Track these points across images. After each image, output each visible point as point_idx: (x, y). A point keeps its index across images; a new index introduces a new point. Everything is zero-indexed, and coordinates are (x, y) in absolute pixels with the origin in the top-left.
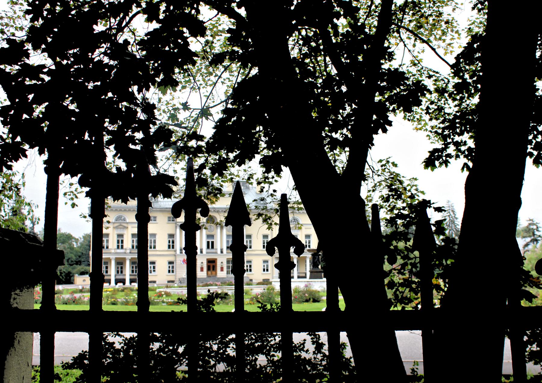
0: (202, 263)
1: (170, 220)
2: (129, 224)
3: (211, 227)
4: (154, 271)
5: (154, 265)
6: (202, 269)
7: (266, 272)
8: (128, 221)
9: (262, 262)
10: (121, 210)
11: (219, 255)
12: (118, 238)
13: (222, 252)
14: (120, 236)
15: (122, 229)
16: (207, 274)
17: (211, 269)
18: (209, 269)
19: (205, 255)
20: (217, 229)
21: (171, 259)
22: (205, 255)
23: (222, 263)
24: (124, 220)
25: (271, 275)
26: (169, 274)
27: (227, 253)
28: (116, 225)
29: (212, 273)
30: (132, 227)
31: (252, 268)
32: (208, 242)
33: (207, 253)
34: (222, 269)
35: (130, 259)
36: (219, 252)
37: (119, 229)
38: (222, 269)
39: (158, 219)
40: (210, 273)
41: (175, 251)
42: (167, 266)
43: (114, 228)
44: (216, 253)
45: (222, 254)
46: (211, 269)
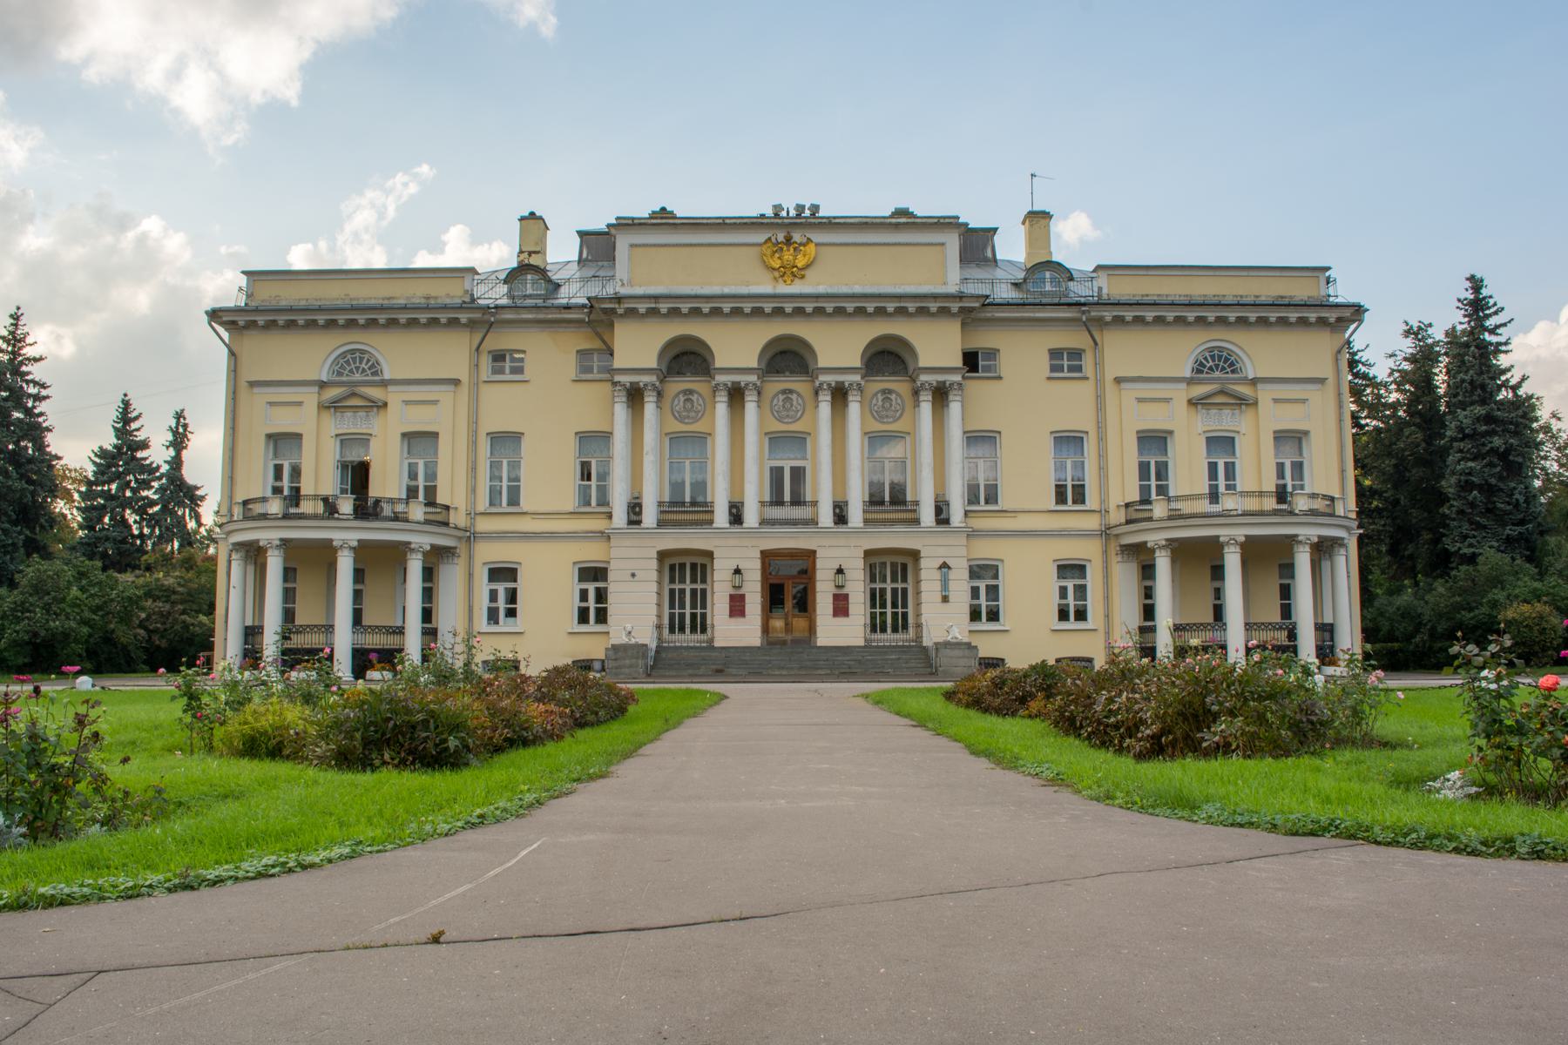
0: (737, 571)
1: (1060, 369)
2: (390, 388)
3: (788, 399)
4: (511, 613)
5: (601, 585)
6: (737, 606)
7: (1072, 624)
8: (387, 376)
9: (1053, 571)
10: (351, 324)
11: (826, 532)
12: (1141, 451)
13: (841, 518)
14: (1221, 443)
15: (362, 414)
16: (766, 629)
17: (789, 603)
18: (774, 596)
19: (751, 533)
20: (917, 404)
21: (591, 553)
22: (751, 533)
23: (840, 571)
24: (375, 369)
25: (1101, 636)
26: (584, 628)
27: (866, 521)
28: (1199, 390)
29: (788, 628)
30: (407, 403)
31: (1005, 603)
32: (777, 473)
33: (764, 522)
34: (841, 606)
35: (354, 549)
36: (826, 517)
37: (1213, 411)
38: (841, 606)
39: (1006, 364)
40: (778, 624)
41: (610, 516)
42: (1054, 584)
43: (323, 407)
44: (813, 522)
45: (842, 529)
46: (789, 603)
